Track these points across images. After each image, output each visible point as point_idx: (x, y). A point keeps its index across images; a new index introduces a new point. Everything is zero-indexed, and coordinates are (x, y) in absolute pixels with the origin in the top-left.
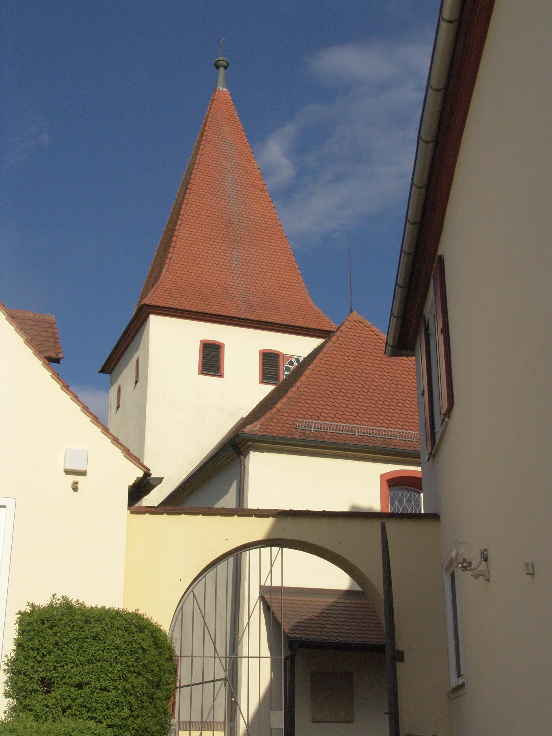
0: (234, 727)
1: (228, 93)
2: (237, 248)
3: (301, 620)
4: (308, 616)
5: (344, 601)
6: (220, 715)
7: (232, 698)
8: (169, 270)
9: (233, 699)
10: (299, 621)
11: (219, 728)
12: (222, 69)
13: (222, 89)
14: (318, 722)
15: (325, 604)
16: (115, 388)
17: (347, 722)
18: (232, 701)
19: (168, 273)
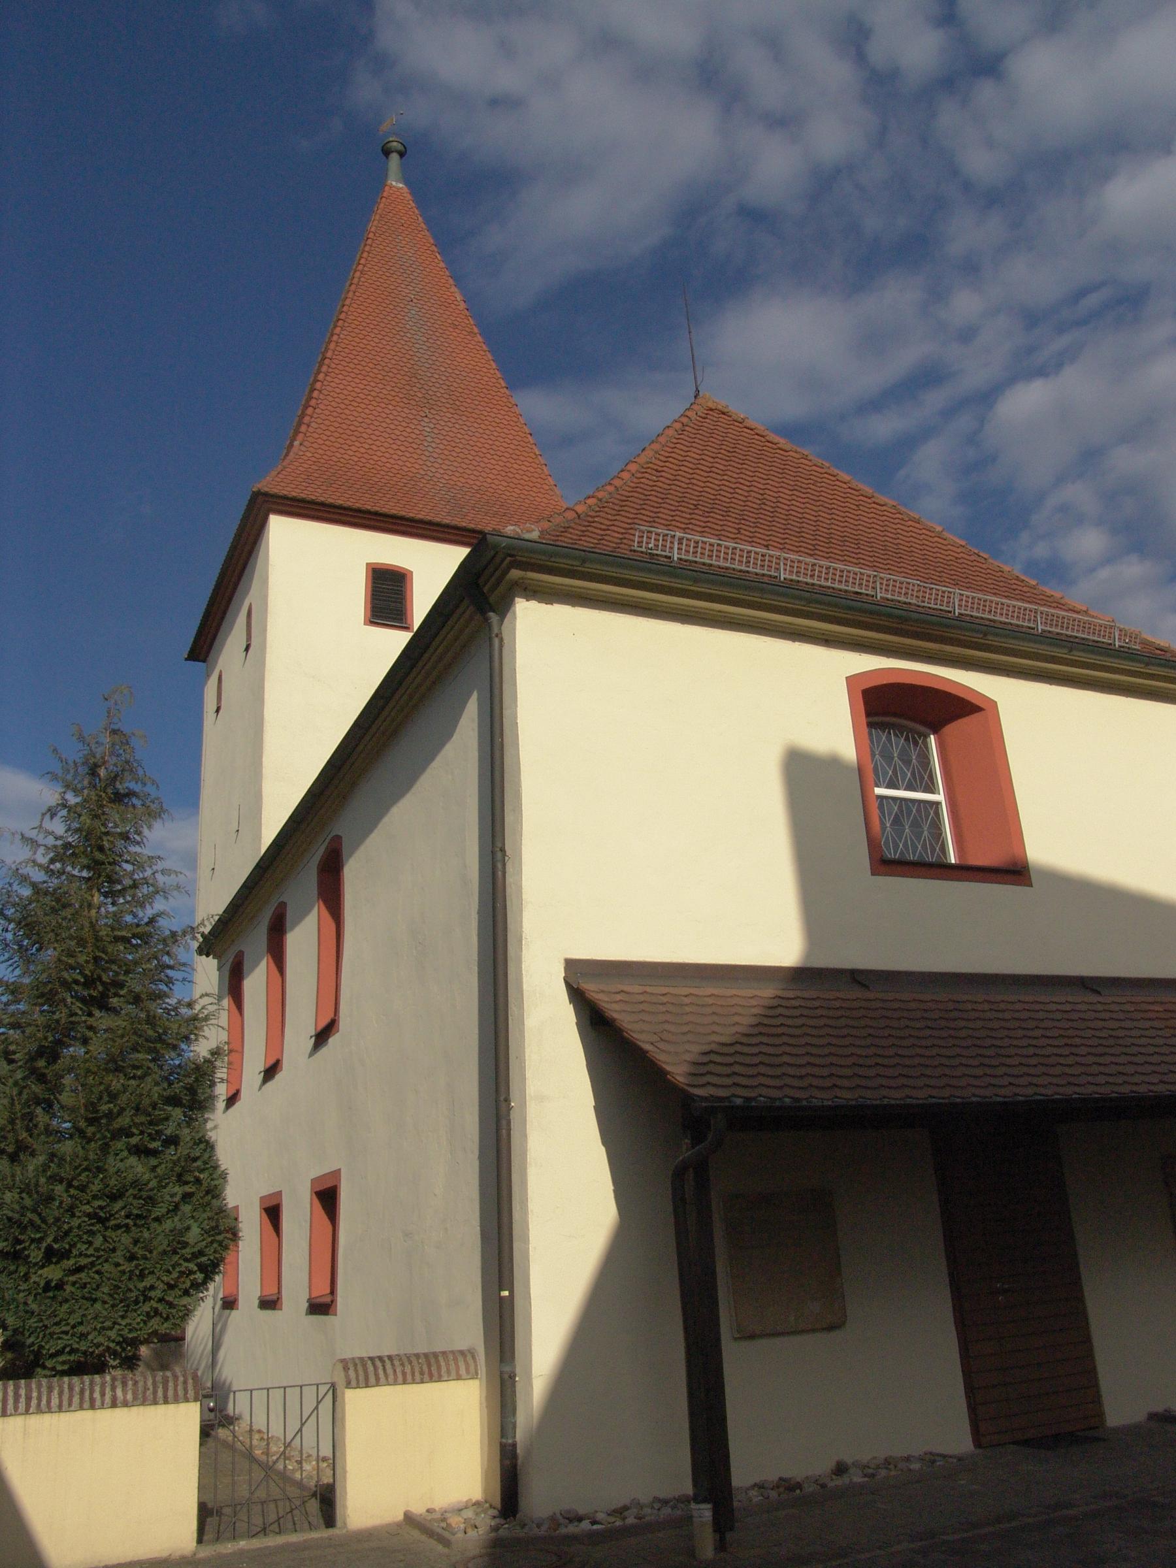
0: (512, 1377)
1: (406, 190)
2: (430, 416)
3: (714, 1047)
4: (725, 1035)
5: (799, 994)
6: (467, 1329)
7: (501, 1289)
8: (306, 443)
9: (506, 1293)
10: (707, 1048)
11: (463, 1371)
12: (394, 157)
13: (395, 183)
14: (752, 1337)
15: (754, 1002)
16: (213, 680)
17: (831, 1328)
18: (501, 1299)
19: (303, 448)
